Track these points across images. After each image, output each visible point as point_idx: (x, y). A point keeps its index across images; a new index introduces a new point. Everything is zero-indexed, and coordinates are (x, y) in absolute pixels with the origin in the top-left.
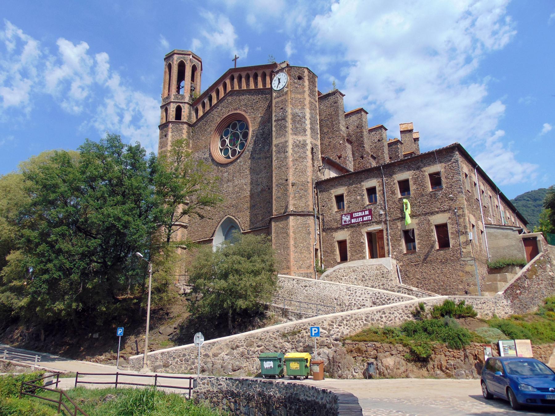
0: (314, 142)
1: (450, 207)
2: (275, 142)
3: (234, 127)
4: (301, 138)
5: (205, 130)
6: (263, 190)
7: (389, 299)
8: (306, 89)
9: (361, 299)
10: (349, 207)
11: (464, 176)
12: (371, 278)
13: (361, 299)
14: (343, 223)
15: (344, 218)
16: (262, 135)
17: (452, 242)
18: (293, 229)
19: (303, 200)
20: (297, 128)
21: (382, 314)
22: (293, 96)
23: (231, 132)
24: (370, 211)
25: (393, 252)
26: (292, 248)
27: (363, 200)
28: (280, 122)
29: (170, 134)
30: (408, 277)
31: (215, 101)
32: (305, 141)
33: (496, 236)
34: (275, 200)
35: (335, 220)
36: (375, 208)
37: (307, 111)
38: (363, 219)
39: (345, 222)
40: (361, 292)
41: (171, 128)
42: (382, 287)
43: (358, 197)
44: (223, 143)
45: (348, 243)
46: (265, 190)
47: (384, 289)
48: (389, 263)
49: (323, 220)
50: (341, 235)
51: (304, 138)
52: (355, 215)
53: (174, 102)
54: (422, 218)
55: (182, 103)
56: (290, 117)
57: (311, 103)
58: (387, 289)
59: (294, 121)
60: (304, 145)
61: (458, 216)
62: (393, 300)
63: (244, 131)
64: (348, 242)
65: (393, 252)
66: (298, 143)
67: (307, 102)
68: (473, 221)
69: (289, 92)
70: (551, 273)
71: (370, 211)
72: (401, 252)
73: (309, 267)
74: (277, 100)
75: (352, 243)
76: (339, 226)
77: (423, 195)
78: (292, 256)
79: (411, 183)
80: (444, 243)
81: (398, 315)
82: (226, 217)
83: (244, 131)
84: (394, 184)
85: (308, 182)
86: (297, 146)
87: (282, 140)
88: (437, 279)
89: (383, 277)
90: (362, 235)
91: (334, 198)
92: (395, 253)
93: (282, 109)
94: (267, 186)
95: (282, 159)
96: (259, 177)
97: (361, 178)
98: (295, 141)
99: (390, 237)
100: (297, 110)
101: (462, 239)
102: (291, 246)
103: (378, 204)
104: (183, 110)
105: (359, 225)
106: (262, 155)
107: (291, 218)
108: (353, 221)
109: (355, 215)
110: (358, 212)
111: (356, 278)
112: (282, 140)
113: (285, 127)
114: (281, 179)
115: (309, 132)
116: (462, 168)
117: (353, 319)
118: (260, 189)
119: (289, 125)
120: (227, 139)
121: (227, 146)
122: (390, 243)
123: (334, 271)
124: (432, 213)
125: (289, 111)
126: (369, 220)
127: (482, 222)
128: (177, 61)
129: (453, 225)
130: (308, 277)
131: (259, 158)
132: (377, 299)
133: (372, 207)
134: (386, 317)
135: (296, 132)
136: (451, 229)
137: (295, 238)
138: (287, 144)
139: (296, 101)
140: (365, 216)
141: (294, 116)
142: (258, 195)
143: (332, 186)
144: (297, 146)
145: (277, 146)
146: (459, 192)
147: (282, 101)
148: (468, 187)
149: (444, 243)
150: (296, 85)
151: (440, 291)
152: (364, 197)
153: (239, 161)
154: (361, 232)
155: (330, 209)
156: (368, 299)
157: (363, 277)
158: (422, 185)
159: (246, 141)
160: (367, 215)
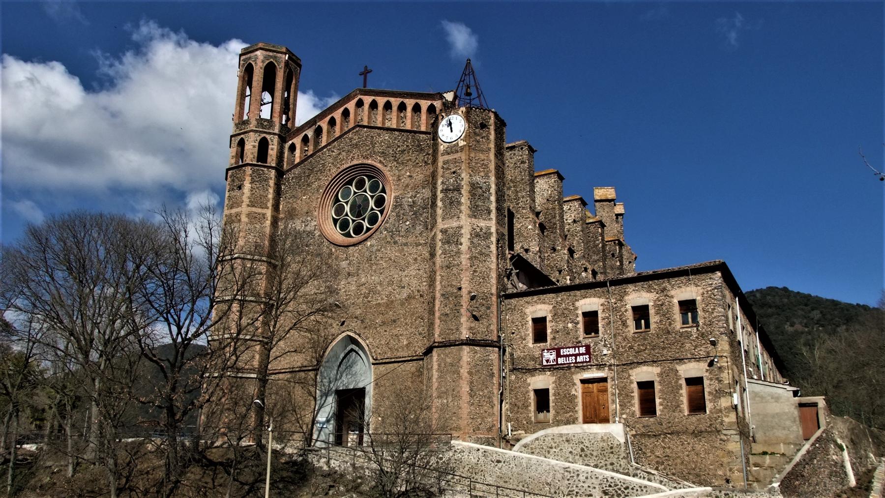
1: (708, 353)
2: (441, 225)
3: (360, 185)
4: (483, 224)
5: (308, 185)
6: (410, 297)
7: (627, 488)
9: (586, 485)
10: (554, 338)
12: (595, 453)
13: (586, 485)
14: (545, 363)
15: (546, 355)
17: (709, 406)
18: (469, 367)
20: (477, 206)
22: (472, 155)
23: (355, 193)
24: (588, 347)
29: (247, 186)
30: (644, 453)
31: (324, 141)
32: (489, 228)
33: (762, 397)
34: (440, 318)
35: (533, 359)
36: (596, 344)
39: (547, 361)
40: (585, 475)
41: (251, 176)
42: (611, 467)
43: (570, 325)
44: (340, 210)
45: (551, 394)
46: (414, 298)
47: (613, 470)
48: (616, 431)
49: (512, 355)
50: (540, 381)
52: (564, 352)
53: (256, 131)
54: (667, 365)
55: (270, 133)
56: (465, 190)
58: (617, 471)
60: (488, 235)
62: (633, 489)
63: (378, 194)
64: (551, 392)
65: (622, 414)
66: (478, 230)
70: (834, 457)
71: (588, 347)
72: (633, 414)
73: (490, 429)
74: (447, 157)
76: (538, 367)
77: (669, 332)
79: (652, 311)
80: (697, 405)
82: (344, 334)
83: (378, 194)
84: (626, 311)
85: (492, 294)
86: (478, 235)
88: (686, 458)
89: (612, 453)
90: (574, 384)
91: (530, 322)
92: (624, 416)
93: (454, 173)
94: (418, 291)
95: (453, 254)
96: (404, 274)
97: (575, 296)
98: (475, 227)
100: (477, 179)
103: (600, 338)
104: (270, 147)
106: (411, 239)
107: (466, 349)
108: (560, 361)
111: (571, 452)
114: (452, 286)
115: (493, 215)
118: (405, 295)
119: (464, 199)
120: (347, 203)
121: (347, 215)
123: (537, 439)
124: (681, 360)
128: (263, 62)
129: (711, 379)
130: (489, 445)
131: (406, 244)
132: (610, 486)
136: (708, 386)
138: (463, 231)
139: (477, 163)
140: (580, 354)
141: (473, 186)
142: (402, 304)
143: (528, 303)
144: (478, 235)
145: (444, 231)
149: (697, 405)
150: (478, 138)
151: (691, 477)
153: (369, 244)
154: (572, 379)
155: (525, 339)
156: (597, 487)
157: (582, 450)
158: (666, 315)
159: (382, 212)
160: (583, 354)
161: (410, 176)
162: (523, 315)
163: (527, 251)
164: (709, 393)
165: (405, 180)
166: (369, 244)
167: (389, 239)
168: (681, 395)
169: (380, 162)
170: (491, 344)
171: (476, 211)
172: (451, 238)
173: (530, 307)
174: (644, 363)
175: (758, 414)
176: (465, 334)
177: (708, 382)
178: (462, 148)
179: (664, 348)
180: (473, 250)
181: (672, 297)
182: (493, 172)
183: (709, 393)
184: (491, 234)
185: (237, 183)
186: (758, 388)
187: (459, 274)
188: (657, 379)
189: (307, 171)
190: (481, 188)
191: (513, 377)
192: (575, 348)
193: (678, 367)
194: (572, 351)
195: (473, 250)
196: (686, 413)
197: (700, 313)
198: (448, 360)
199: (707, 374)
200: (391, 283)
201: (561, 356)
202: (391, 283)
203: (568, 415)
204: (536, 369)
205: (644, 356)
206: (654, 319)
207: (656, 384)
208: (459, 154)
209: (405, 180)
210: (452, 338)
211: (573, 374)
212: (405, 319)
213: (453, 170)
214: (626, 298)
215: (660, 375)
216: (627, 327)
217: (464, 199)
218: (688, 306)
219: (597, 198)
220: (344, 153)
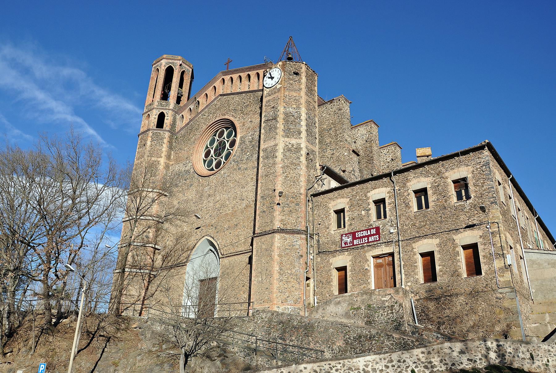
0: (311, 147)
4: (294, 141)
8: (303, 86)
10: (351, 225)
11: (497, 184)
14: (343, 245)
15: (345, 239)
16: (251, 142)
19: (294, 215)
20: (290, 129)
21: (389, 362)
22: (287, 93)
25: (407, 282)
26: (276, 276)
27: (368, 215)
28: (270, 123)
32: (299, 144)
33: (539, 264)
35: (334, 243)
37: (303, 111)
38: (368, 239)
43: (363, 212)
51: (298, 141)
57: (308, 103)
59: (286, 120)
60: (298, 149)
61: (492, 233)
65: (407, 282)
66: (290, 146)
67: (303, 101)
68: (511, 242)
69: (283, 89)
71: (378, 229)
72: (417, 281)
74: (268, 98)
75: (353, 270)
76: (338, 249)
77: (445, 208)
78: (276, 285)
80: (475, 268)
81: (411, 364)
84: (409, 194)
85: (301, 194)
86: (289, 150)
87: (272, 143)
90: (367, 260)
92: (409, 284)
93: (273, 107)
96: (244, 190)
98: (287, 144)
99: (402, 263)
101: (498, 264)
102: (276, 272)
104: (166, 118)
105: (363, 247)
107: (277, 236)
108: (356, 242)
109: (359, 235)
110: (363, 231)
112: (272, 143)
113: (276, 128)
114: (268, 189)
115: (304, 135)
116: (494, 174)
117: (345, 368)
119: (280, 125)
121: (212, 156)
122: (403, 271)
125: (281, 109)
126: (376, 241)
127: (521, 246)
128: (165, 66)
129: (485, 244)
131: (246, 169)
133: (379, 223)
134: (393, 366)
135: (288, 133)
137: (281, 263)
138: (277, 148)
139: (290, 99)
140: (371, 235)
141: (287, 115)
142: (242, 212)
144: (289, 150)
145: (265, 150)
146: (492, 203)
147: (274, 99)
148: (503, 199)
149: (475, 268)
150: (291, 82)
152: (370, 212)
153: (223, 172)
154: (365, 256)
155: (328, 228)
158: (443, 195)
160: (374, 235)
161: (251, 121)
162: (327, 208)
163: (344, 171)
164: (484, 256)
165: (248, 125)
166: (223, 172)
167: (235, 167)
168: (459, 261)
169: (233, 116)
170: (298, 232)
171: (288, 133)
172: (272, 153)
173: (332, 202)
174: (426, 236)
175: (537, 280)
176: (277, 225)
177: (483, 247)
178: (279, 90)
179: (441, 222)
180: (286, 161)
181: (447, 178)
182: (303, 104)
183: (484, 256)
184: (301, 148)
185: (143, 142)
186: (535, 256)
187: (274, 179)
188: (436, 250)
189: (189, 131)
190: (293, 116)
191: (319, 259)
192: (367, 230)
193: (455, 237)
194: (365, 233)
195: (286, 161)
196: (465, 275)
197: (471, 188)
198: (264, 247)
199: (481, 240)
200: (235, 198)
201: (356, 239)
202: (235, 198)
203: (362, 287)
204: (336, 251)
205: (425, 230)
206: (432, 198)
207: (435, 254)
208: (277, 94)
209: (248, 125)
210: (267, 229)
211: (366, 252)
212: (243, 223)
213: (273, 106)
214: (408, 184)
215: (439, 245)
216: (409, 208)
217: (280, 125)
218: (461, 184)
219: (419, 155)
220: (211, 115)
